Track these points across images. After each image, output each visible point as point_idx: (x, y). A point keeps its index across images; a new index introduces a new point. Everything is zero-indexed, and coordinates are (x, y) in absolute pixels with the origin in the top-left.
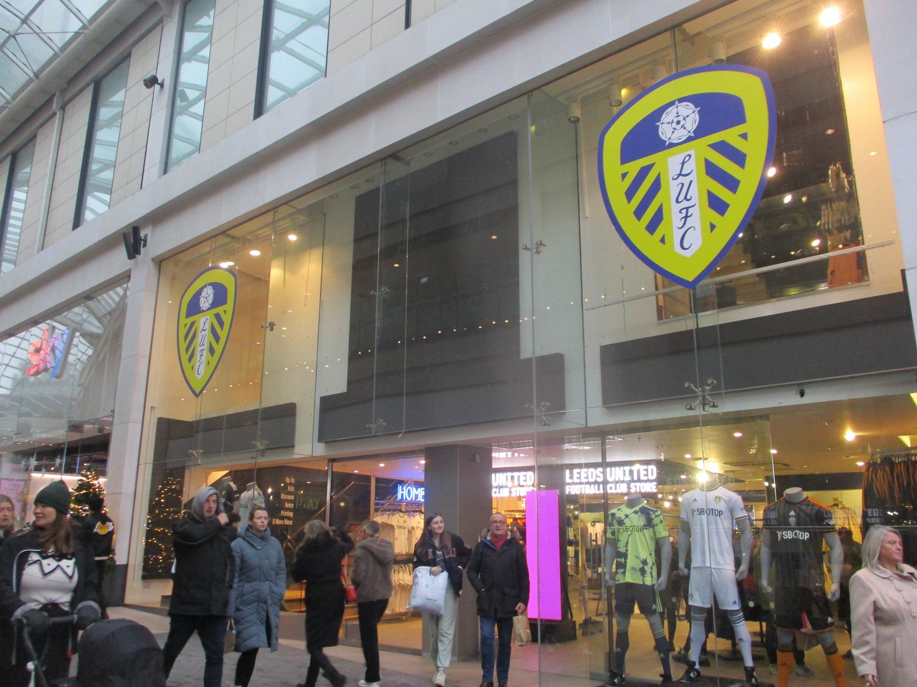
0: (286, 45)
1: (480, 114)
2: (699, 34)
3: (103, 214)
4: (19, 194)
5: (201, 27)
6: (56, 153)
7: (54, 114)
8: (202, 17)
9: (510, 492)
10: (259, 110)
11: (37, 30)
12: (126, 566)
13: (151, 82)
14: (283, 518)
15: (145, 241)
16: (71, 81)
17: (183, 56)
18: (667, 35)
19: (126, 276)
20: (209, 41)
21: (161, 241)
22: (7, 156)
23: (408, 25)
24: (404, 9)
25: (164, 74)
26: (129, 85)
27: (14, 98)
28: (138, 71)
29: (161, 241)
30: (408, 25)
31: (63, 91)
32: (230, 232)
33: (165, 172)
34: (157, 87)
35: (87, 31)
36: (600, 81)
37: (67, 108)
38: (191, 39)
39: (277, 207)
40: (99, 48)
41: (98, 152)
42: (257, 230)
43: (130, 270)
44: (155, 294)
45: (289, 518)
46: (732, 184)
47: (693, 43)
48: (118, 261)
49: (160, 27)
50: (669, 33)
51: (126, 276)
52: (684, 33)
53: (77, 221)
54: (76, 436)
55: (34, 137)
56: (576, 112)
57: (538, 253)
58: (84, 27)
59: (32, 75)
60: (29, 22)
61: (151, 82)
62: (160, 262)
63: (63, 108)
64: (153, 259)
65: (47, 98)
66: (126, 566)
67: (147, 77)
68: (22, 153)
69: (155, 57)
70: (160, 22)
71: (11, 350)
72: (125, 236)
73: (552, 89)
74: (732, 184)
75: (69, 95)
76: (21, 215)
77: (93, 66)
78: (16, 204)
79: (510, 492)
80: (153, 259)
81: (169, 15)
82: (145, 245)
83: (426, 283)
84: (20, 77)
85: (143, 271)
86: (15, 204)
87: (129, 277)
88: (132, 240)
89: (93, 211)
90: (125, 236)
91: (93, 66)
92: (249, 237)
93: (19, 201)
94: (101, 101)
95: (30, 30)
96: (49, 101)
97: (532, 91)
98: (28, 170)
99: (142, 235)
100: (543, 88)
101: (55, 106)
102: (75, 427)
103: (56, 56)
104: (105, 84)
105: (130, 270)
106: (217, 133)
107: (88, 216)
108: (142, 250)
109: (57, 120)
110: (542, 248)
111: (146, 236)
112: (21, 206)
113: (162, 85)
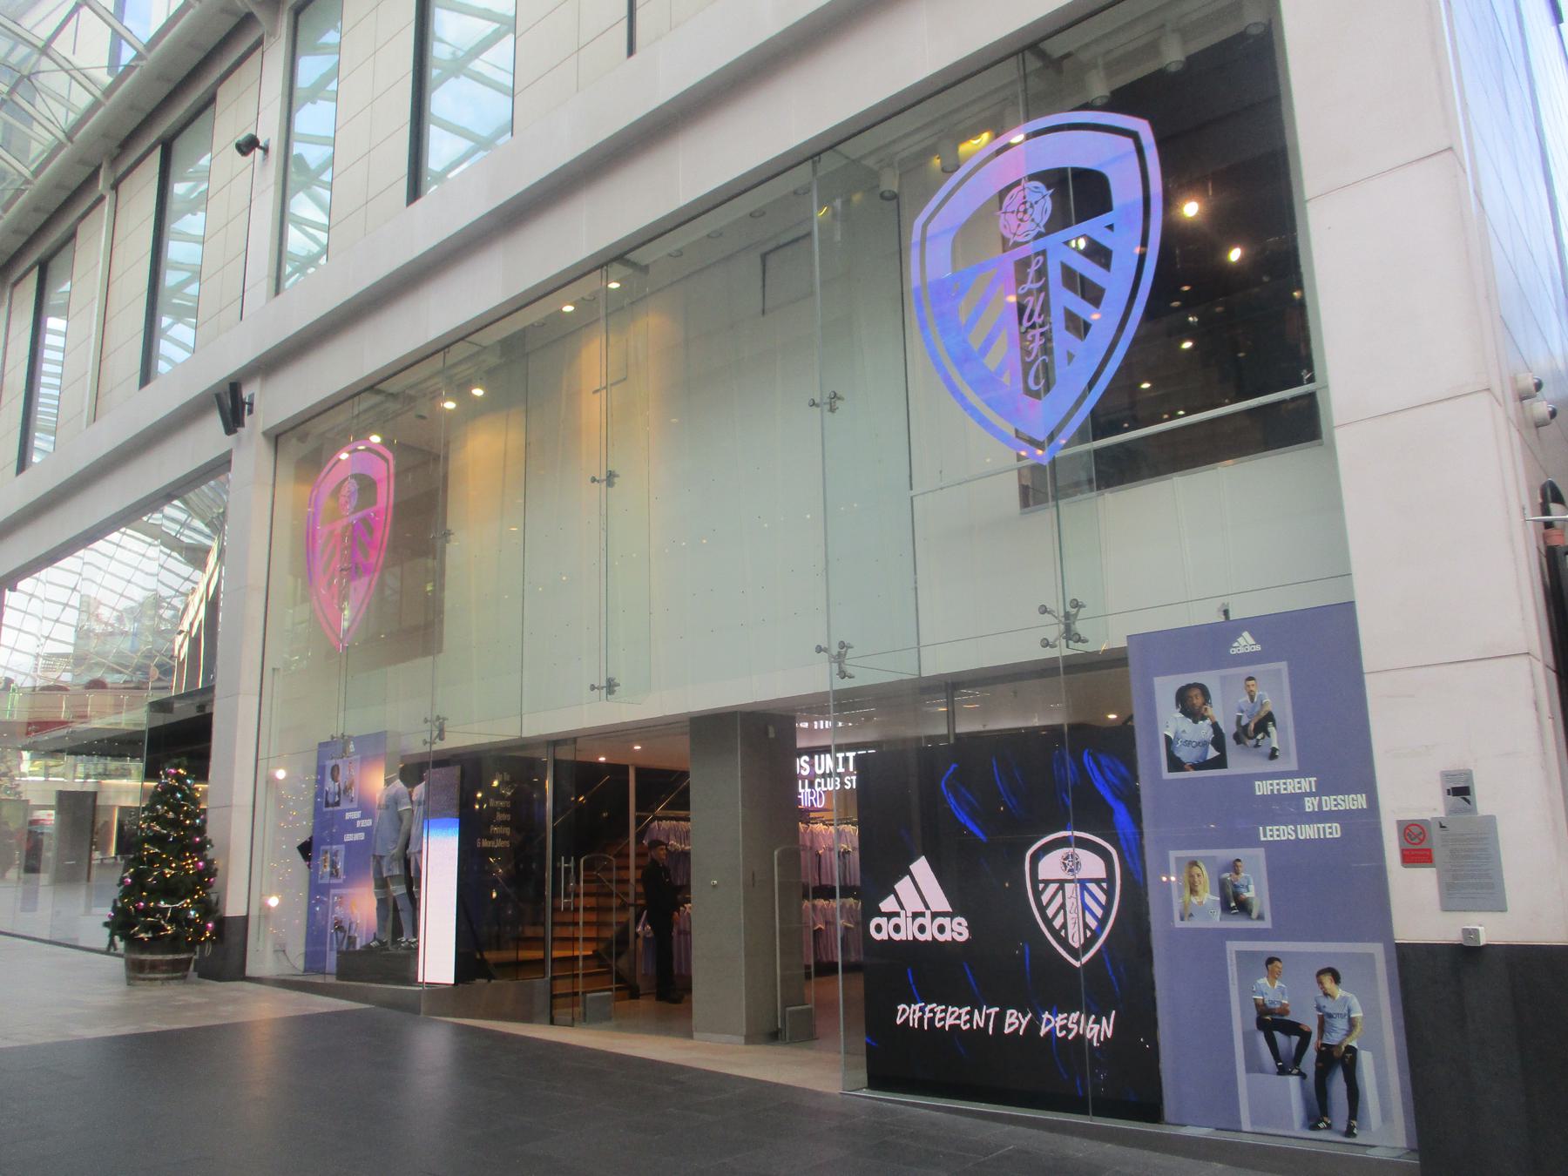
0: (470, 66)
1: (860, 132)
2: (1068, 55)
3: (190, 356)
4: (53, 323)
5: (327, 46)
6: (108, 251)
7: (101, 199)
8: (327, 31)
9: (843, 783)
10: (415, 191)
11: (67, 66)
12: (246, 919)
13: (248, 146)
14: (491, 838)
15: (251, 404)
16: (126, 144)
17: (298, 95)
18: (808, 166)
19: (222, 465)
20: (335, 72)
21: (275, 402)
22: (31, 269)
23: (631, 51)
24: (625, 23)
25: (269, 132)
26: (216, 148)
27: (36, 173)
28: (228, 124)
29: (275, 402)
30: (631, 51)
31: (114, 161)
32: (381, 387)
33: (277, 292)
34: (258, 152)
35: (143, 63)
36: (917, 137)
37: (123, 187)
38: (310, 68)
39: (448, 346)
40: (167, 88)
41: (175, 250)
42: (425, 380)
43: (229, 453)
44: (270, 489)
45: (503, 837)
46: (1093, 294)
47: (1059, 71)
48: (209, 437)
49: (258, 53)
50: (1013, 60)
51: (222, 465)
52: (1042, 55)
53: (146, 376)
54: (161, 720)
55: (71, 236)
56: (890, 183)
57: (832, 410)
58: (139, 56)
59: (61, 136)
60: (51, 53)
61: (248, 146)
62: (276, 437)
63: (115, 187)
64: (265, 434)
65: (89, 170)
66: (246, 919)
67: (241, 138)
68: (52, 264)
69: (249, 102)
70: (259, 43)
71: (71, 580)
72: (218, 396)
73: (851, 149)
74: (1093, 294)
75: (122, 168)
76: (59, 356)
77: (160, 115)
78: (52, 339)
79: (843, 783)
80: (265, 434)
81: (273, 34)
82: (250, 412)
83: (1187, 351)
84: (41, 140)
85: (250, 454)
86: (49, 339)
87: (230, 462)
88: (230, 404)
89: (169, 360)
90: (218, 396)
91: (160, 115)
92: (412, 392)
93: (56, 333)
94: (175, 169)
95: (55, 67)
96: (93, 178)
97: (819, 154)
98: (67, 287)
99: (245, 394)
100: (840, 147)
101: (102, 185)
102: (161, 706)
103: (96, 105)
104: (180, 146)
105: (229, 453)
106: (342, 230)
107: (163, 367)
108: (247, 419)
109: (106, 207)
110: (838, 403)
111: (252, 396)
112: (59, 341)
113: (266, 150)
